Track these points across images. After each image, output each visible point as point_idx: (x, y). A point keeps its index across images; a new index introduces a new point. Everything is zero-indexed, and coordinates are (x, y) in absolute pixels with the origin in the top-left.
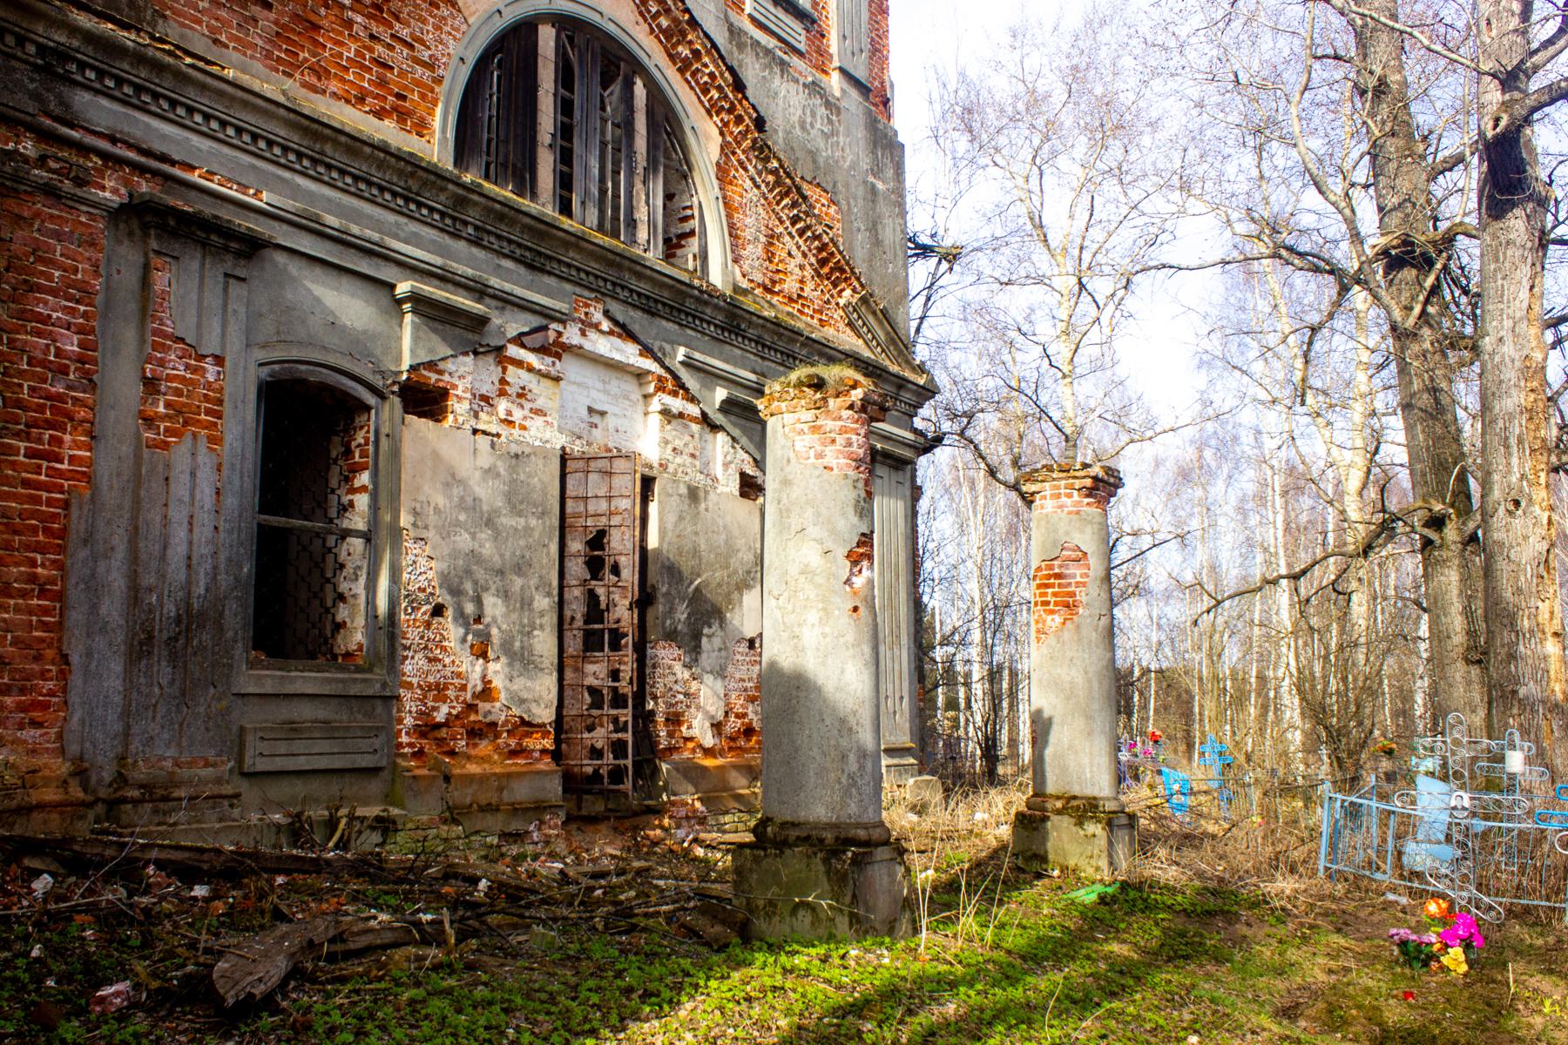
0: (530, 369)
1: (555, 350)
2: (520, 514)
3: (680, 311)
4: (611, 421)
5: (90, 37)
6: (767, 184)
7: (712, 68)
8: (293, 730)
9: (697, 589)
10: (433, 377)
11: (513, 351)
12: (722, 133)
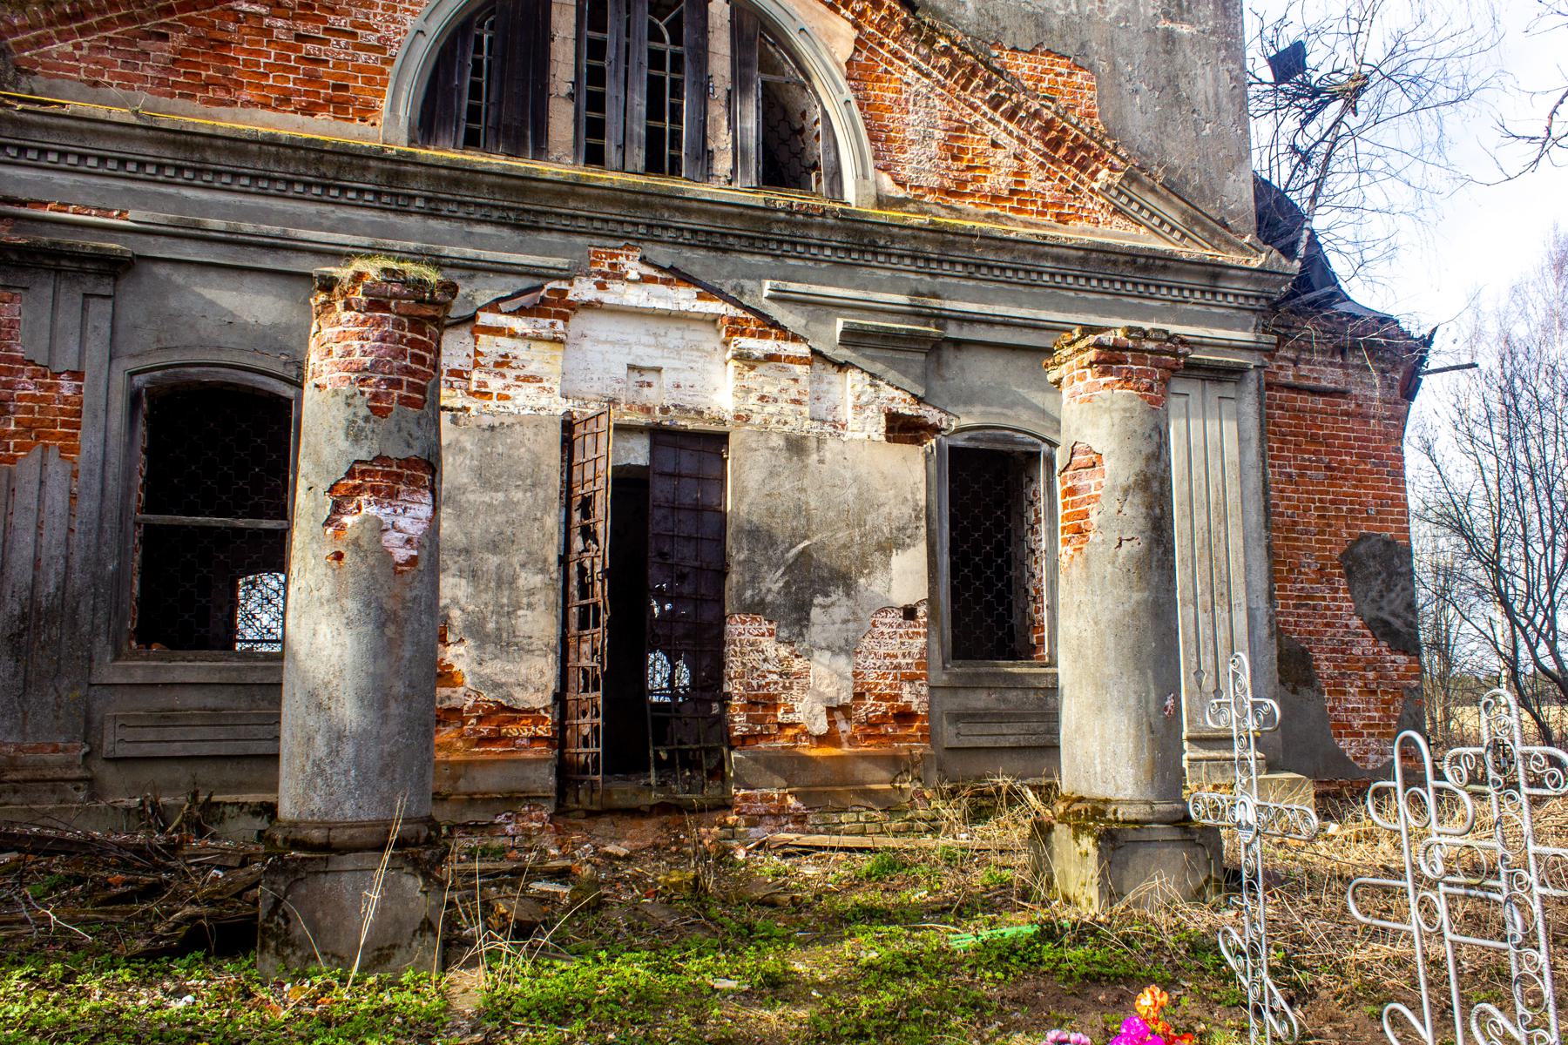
0: (513, 335)
1: (561, 308)
2: (496, 489)
4: (667, 378)
8: (167, 718)
9: (803, 552)
11: (486, 319)
12: (857, 26)
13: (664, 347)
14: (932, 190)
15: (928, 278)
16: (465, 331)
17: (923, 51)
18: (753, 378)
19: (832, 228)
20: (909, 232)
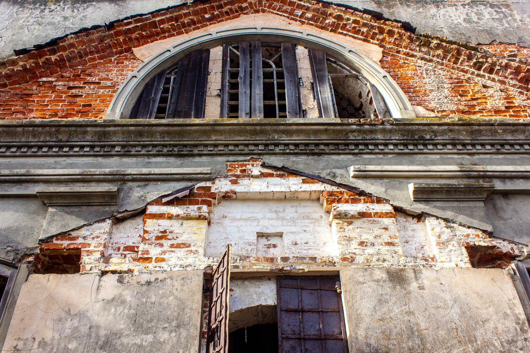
0: (170, 217)
1: (209, 198)
2: (147, 332)
3: (347, 145)
4: (287, 240)
6: (438, 56)
7: (353, 18)
10: (65, 243)
11: (152, 209)
12: (381, 46)
13: (283, 219)
14: (453, 112)
15: (468, 157)
16: (139, 220)
17: (424, 49)
18: (352, 230)
19: (390, 131)
20: (446, 127)
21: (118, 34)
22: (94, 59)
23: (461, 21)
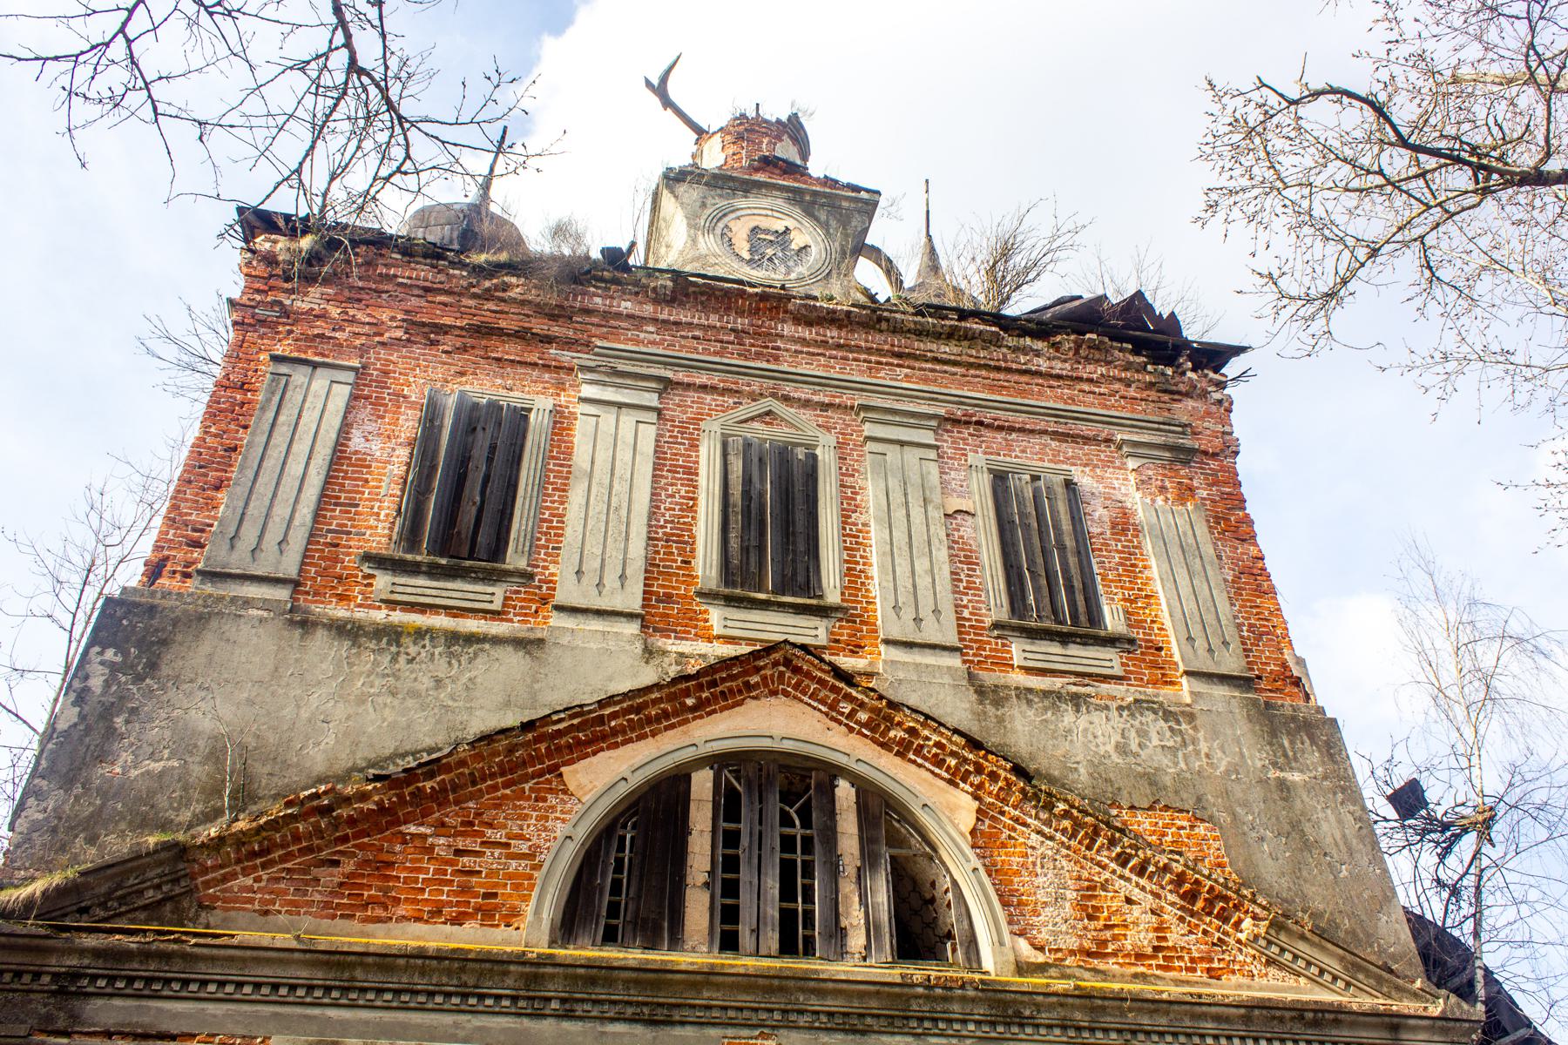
5: (97, 953)
6: (1064, 831)
7: (935, 738)
12: (976, 798)
14: (1072, 953)
17: (1044, 815)
19: (973, 1000)
20: (1054, 999)
21: (537, 740)
22: (495, 788)
23: (1110, 748)
